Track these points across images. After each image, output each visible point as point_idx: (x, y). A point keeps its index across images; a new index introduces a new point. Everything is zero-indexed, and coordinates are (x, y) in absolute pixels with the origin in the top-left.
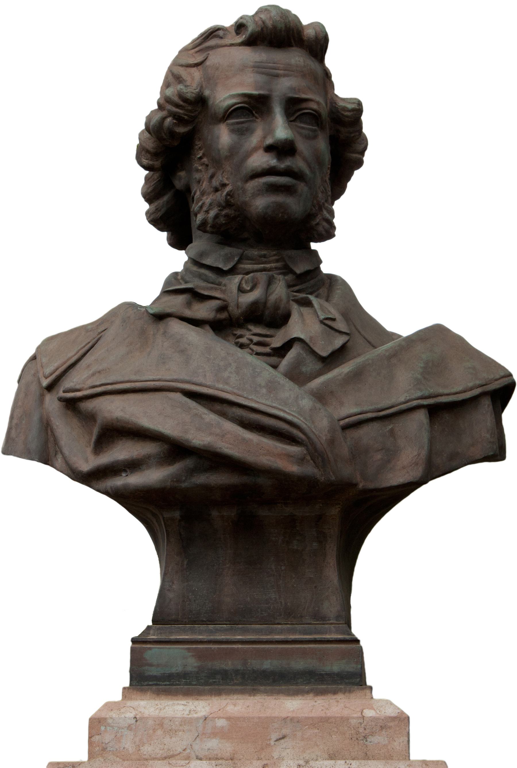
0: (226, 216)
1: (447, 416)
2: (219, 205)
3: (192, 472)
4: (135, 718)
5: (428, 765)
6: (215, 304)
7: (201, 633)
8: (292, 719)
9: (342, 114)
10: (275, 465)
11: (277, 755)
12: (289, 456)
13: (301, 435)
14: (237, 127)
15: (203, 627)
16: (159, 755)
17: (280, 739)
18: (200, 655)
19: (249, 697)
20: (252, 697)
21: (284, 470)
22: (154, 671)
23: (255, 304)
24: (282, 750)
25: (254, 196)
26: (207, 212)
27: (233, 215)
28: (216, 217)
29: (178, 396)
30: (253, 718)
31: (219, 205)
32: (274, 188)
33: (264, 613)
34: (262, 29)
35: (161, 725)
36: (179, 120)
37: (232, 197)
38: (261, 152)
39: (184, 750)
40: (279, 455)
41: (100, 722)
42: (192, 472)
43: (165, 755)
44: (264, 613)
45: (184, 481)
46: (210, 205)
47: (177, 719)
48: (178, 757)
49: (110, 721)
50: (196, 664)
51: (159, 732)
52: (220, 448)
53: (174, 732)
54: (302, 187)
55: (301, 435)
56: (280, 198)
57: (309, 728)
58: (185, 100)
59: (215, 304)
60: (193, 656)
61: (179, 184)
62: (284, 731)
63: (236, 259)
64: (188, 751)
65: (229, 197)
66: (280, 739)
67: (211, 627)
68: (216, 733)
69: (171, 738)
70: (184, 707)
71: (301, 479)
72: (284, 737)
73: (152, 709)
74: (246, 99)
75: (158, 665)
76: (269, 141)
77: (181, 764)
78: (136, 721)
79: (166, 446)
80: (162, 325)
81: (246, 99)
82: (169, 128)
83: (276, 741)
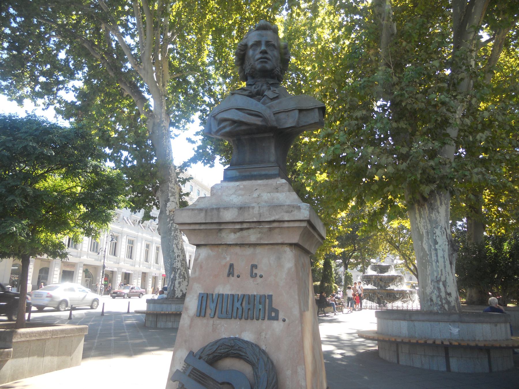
1: (305, 112)
6: (248, 91)
23: (258, 90)
28: (249, 71)
32: (262, 62)
36: (241, 50)
54: (269, 62)
56: (264, 64)
58: (242, 45)
59: (248, 91)
62: (257, 188)
68: (240, 189)
72: (257, 189)
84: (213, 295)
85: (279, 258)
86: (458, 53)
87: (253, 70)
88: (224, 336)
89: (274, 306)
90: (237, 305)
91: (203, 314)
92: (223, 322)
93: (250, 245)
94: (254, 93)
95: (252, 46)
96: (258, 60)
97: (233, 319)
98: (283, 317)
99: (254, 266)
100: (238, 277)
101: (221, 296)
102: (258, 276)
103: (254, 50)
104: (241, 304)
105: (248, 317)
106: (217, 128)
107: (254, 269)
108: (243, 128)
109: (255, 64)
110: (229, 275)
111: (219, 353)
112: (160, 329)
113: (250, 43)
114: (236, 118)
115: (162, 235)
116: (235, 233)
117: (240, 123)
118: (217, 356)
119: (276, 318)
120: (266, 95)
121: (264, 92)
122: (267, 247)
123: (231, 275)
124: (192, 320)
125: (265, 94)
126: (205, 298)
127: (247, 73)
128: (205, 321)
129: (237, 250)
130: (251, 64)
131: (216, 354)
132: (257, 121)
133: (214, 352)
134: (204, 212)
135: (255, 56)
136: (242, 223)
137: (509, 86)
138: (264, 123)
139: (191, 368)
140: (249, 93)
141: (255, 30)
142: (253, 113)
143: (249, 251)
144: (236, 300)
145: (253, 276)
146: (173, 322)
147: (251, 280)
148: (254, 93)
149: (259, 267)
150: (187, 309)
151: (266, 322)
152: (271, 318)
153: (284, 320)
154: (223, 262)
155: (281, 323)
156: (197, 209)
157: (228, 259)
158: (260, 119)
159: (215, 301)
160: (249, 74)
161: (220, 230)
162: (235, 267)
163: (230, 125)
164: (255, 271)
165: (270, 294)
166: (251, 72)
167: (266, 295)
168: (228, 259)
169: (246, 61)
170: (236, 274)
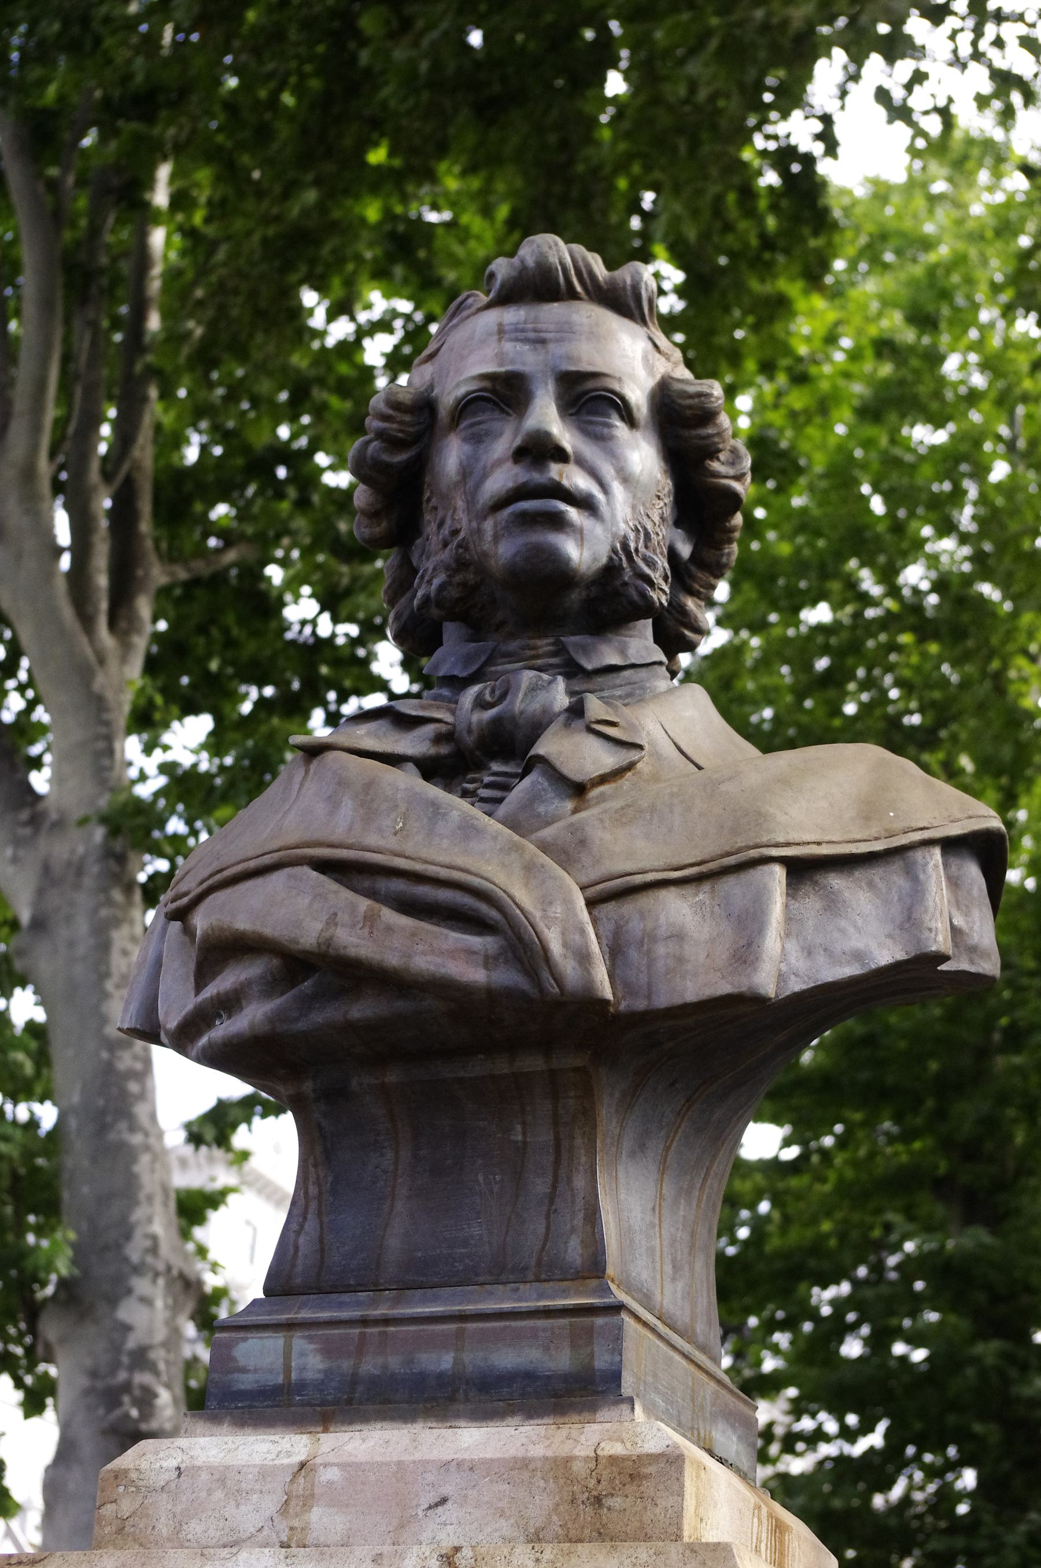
0: (464, 585)
2: (447, 568)
3: (306, 1004)
4: (179, 1468)
5: (695, 1552)
7: (341, 1306)
8: (460, 1464)
9: (680, 405)
10: (443, 970)
13: (494, 914)
14: (470, 431)
15: (346, 1297)
16: (214, 1541)
17: (437, 1505)
18: (328, 1351)
19: (404, 1426)
20: (409, 1425)
21: (459, 979)
22: (246, 1382)
24: (439, 1527)
26: (430, 582)
27: (473, 582)
28: (442, 587)
30: (387, 1464)
31: (447, 568)
33: (457, 1264)
34: (520, 272)
35: (222, 1481)
37: (467, 549)
39: (260, 1530)
40: (452, 954)
41: (116, 1477)
42: (306, 1004)
43: (225, 1540)
44: (457, 1264)
45: (297, 1020)
46: (434, 569)
47: (251, 1469)
48: (248, 1543)
49: (133, 1475)
50: (321, 1366)
51: (219, 1494)
52: (345, 947)
53: (244, 1495)
55: (494, 914)
57: (491, 1481)
59: (429, 729)
60: (317, 1350)
62: (447, 1490)
63: (483, 658)
64: (265, 1532)
65: (461, 551)
66: (437, 1505)
67: (362, 1296)
69: (238, 1506)
70: (272, 1447)
71: (492, 995)
72: (443, 1501)
73: (214, 1452)
74: (486, 384)
75: (256, 1371)
77: (222, 1556)
78: (179, 1476)
79: (275, 961)
80: (315, 764)
81: (486, 384)
82: (372, 458)
83: (430, 1507)
86: (1016, 588)
87: (470, 577)
94: (470, 740)
95: (466, 406)
103: (477, 439)
106: (190, 1002)
109: (479, 531)
113: (450, 394)
120: (541, 759)
121: (537, 728)
125: (542, 748)
127: (427, 599)
130: (455, 532)
135: (485, 476)
137: (747, 192)
138: (506, 977)
140: (438, 739)
142: (444, 895)
148: (470, 740)
158: (476, 941)
160: (439, 604)
163: (272, 986)
166: (454, 593)
169: (427, 517)
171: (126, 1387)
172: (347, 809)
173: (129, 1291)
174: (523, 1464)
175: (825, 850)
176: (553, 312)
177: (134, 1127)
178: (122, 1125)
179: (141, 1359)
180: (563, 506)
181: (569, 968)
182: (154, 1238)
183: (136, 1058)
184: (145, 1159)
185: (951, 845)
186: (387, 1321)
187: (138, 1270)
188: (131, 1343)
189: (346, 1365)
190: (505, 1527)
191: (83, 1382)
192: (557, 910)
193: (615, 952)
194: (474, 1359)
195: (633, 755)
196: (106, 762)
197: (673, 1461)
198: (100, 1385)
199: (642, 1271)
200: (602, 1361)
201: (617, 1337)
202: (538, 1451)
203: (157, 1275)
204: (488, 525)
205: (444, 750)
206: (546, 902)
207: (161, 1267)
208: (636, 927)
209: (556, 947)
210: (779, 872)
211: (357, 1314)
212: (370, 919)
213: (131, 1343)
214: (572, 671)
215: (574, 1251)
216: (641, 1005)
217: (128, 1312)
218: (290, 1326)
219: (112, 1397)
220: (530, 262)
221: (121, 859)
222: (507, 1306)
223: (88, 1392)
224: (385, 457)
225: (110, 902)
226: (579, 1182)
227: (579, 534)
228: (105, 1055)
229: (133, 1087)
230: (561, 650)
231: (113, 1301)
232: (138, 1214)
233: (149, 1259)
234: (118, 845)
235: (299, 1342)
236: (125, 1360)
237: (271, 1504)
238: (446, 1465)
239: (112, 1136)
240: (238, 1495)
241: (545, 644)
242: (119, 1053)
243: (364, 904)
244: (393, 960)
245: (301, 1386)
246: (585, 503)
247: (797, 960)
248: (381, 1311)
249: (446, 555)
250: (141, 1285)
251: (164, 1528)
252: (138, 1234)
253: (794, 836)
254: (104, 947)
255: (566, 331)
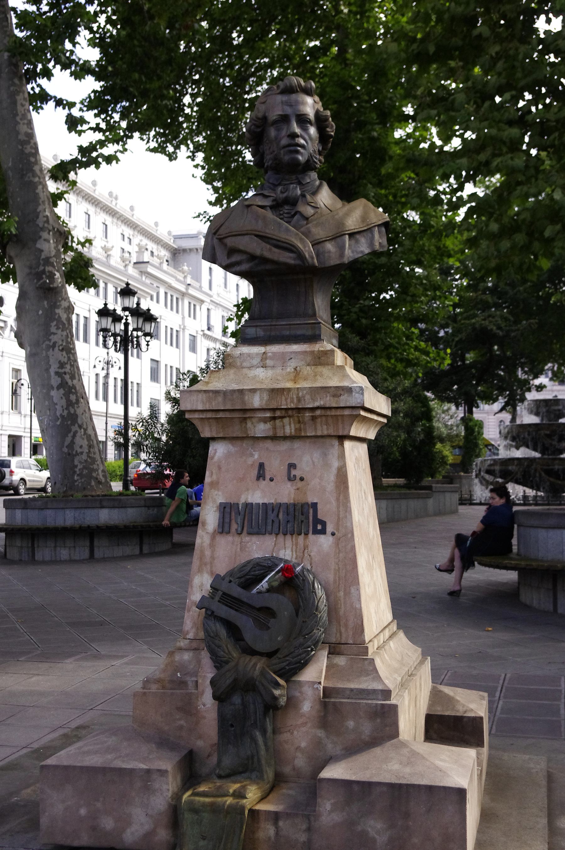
6: (272, 198)
11: (103, 369)
12: (291, 258)
22: (249, 337)
25: (284, 155)
29: (253, 236)
38: (286, 138)
58: (259, 119)
59: (272, 198)
61: (261, 151)
71: (295, 266)
76: (288, 133)
80: (249, 209)
84: (238, 504)
85: (325, 455)
88: (256, 556)
89: (320, 516)
90: (272, 516)
91: (226, 529)
92: (254, 539)
93: (285, 438)
95: (275, 122)
96: (284, 147)
97: (267, 535)
98: (332, 530)
99: (292, 466)
100: (272, 480)
101: (248, 506)
102: (298, 478)
104: (278, 516)
105: (287, 531)
107: (292, 469)
108: (268, 267)
110: (258, 478)
111: (253, 575)
112: (44, 563)
114: (258, 252)
115: (27, 345)
116: (265, 422)
117: (264, 260)
118: (250, 579)
119: (323, 532)
122: (308, 441)
123: (261, 478)
124: (213, 537)
126: (228, 510)
128: (230, 538)
129: (269, 444)
131: (248, 577)
132: (286, 258)
133: (247, 574)
134: (222, 395)
136: (274, 410)
138: (298, 262)
139: (220, 593)
140: (273, 201)
141: (278, 94)
142: (285, 245)
143: (284, 446)
144: (270, 512)
145: (291, 478)
146: (70, 548)
147: (289, 484)
149: (298, 466)
150: (204, 524)
151: (311, 537)
152: (316, 532)
153: (333, 534)
154: (250, 461)
155: (331, 539)
156: (212, 391)
157: (256, 457)
158: (292, 255)
159: (242, 513)
161: (245, 419)
162: (266, 467)
164: (293, 472)
165: (315, 501)
167: (310, 503)
168: (256, 457)
170: (268, 477)
171: (44, 272)
172: (260, 222)
173: (40, 237)
174: (306, 352)
175: (356, 231)
176: (294, 96)
177: (34, 175)
178: (30, 174)
179: (47, 261)
180: (299, 148)
181: (310, 260)
182: (47, 217)
183: (31, 147)
184: (40, 187)
185: (379, 226)
186: (275, 325)
187: (42, 229)
188: (43, 257)
189: (268, 333)
190: (303, 363)
191: (27, 270)
192: (307, 248)
193: (318, 255)
194: (293, 332)
195: (317, 210)
196: (4, 24)
197: (332, 351)
198: (33, 271)
199: (321, 313)
200: (317, 333)
201: (320, 328)
202: (308, 350)
203: (50, 231)
204: (282, 152)
205: (274, 203)
206: (305, 247)
207: (51, 228)
208: (321, 250)
209: (307, 256)
210: (347, 236)
211: (269, 324)
212: (270, 250)
213: (43, 257)
214: (300, 183)
215: (310, 312)
216: (323, 266)
217: (41, 245)
218: (256, 326)
219: (39, 275)
220: (288, 84)
221: (16, 66)
222: (299, 322)
223: (29, 274)
224: (255, 130)
225: (14, 84)
226: (310, 298)
227: (302, 154)
228: (20, 147)
229: (33, 160)
230: (297, 178)
231: (35, 241)
232: (40, 208)
233: (46, 225)
234: (14, 61)
235: (258, 329)
236: (42, 262)
237: (259, 360)
238: (291, 352)
239: (26, 179)
240: (252, 358)
241: (294, 177)
242: (25, 146)
243: (268, 246)
244: (276, 258)
245: (260, 337)
246: (303, 146)
247: (351, 255)
248: (274, 323)
249: (271, 156)
250: (45, 235)
251: (239, 364)
252: (41, 215)
253: (351, 228)
254: (14, 103)
255: (297, 103)
